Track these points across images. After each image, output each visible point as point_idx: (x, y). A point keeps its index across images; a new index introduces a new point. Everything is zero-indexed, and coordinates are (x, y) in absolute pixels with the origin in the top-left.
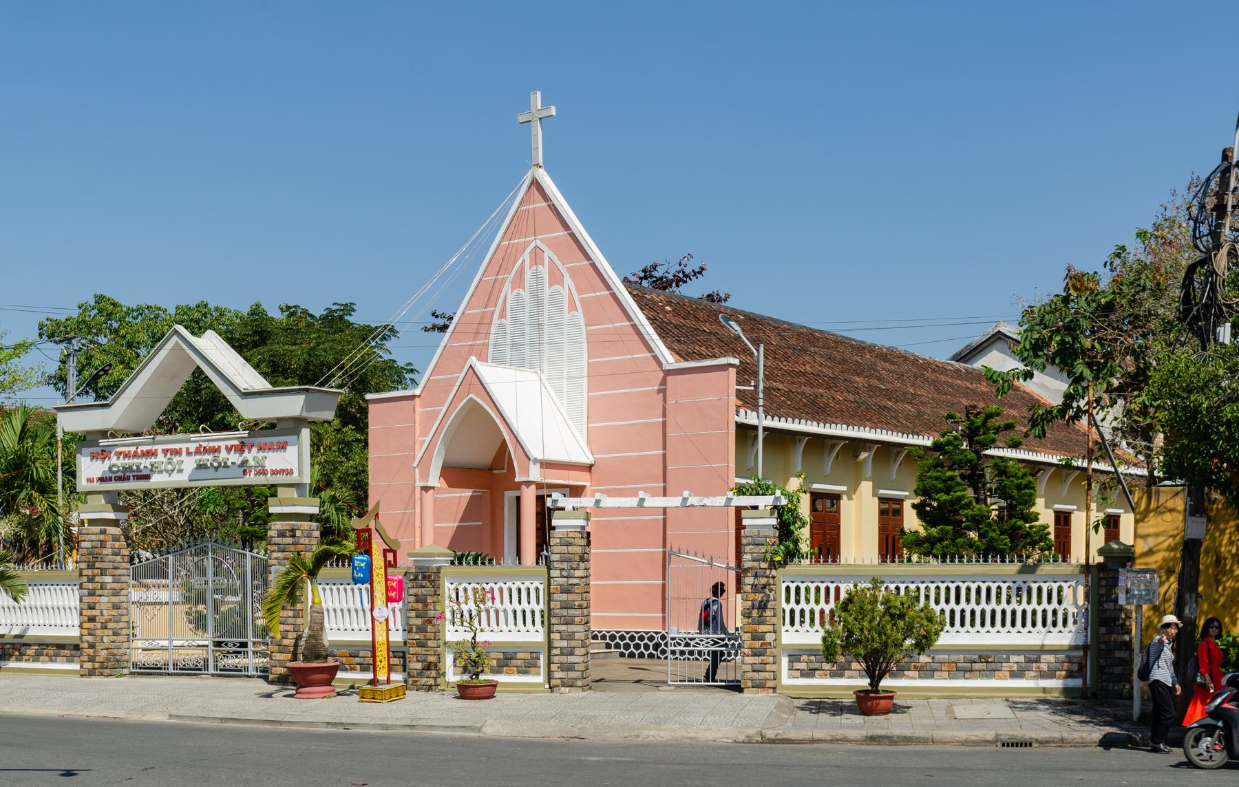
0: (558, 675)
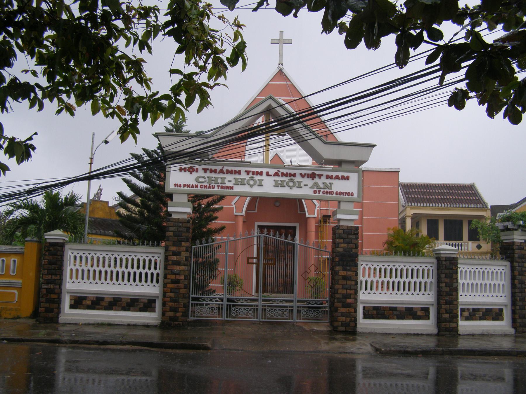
0: (519, 321)
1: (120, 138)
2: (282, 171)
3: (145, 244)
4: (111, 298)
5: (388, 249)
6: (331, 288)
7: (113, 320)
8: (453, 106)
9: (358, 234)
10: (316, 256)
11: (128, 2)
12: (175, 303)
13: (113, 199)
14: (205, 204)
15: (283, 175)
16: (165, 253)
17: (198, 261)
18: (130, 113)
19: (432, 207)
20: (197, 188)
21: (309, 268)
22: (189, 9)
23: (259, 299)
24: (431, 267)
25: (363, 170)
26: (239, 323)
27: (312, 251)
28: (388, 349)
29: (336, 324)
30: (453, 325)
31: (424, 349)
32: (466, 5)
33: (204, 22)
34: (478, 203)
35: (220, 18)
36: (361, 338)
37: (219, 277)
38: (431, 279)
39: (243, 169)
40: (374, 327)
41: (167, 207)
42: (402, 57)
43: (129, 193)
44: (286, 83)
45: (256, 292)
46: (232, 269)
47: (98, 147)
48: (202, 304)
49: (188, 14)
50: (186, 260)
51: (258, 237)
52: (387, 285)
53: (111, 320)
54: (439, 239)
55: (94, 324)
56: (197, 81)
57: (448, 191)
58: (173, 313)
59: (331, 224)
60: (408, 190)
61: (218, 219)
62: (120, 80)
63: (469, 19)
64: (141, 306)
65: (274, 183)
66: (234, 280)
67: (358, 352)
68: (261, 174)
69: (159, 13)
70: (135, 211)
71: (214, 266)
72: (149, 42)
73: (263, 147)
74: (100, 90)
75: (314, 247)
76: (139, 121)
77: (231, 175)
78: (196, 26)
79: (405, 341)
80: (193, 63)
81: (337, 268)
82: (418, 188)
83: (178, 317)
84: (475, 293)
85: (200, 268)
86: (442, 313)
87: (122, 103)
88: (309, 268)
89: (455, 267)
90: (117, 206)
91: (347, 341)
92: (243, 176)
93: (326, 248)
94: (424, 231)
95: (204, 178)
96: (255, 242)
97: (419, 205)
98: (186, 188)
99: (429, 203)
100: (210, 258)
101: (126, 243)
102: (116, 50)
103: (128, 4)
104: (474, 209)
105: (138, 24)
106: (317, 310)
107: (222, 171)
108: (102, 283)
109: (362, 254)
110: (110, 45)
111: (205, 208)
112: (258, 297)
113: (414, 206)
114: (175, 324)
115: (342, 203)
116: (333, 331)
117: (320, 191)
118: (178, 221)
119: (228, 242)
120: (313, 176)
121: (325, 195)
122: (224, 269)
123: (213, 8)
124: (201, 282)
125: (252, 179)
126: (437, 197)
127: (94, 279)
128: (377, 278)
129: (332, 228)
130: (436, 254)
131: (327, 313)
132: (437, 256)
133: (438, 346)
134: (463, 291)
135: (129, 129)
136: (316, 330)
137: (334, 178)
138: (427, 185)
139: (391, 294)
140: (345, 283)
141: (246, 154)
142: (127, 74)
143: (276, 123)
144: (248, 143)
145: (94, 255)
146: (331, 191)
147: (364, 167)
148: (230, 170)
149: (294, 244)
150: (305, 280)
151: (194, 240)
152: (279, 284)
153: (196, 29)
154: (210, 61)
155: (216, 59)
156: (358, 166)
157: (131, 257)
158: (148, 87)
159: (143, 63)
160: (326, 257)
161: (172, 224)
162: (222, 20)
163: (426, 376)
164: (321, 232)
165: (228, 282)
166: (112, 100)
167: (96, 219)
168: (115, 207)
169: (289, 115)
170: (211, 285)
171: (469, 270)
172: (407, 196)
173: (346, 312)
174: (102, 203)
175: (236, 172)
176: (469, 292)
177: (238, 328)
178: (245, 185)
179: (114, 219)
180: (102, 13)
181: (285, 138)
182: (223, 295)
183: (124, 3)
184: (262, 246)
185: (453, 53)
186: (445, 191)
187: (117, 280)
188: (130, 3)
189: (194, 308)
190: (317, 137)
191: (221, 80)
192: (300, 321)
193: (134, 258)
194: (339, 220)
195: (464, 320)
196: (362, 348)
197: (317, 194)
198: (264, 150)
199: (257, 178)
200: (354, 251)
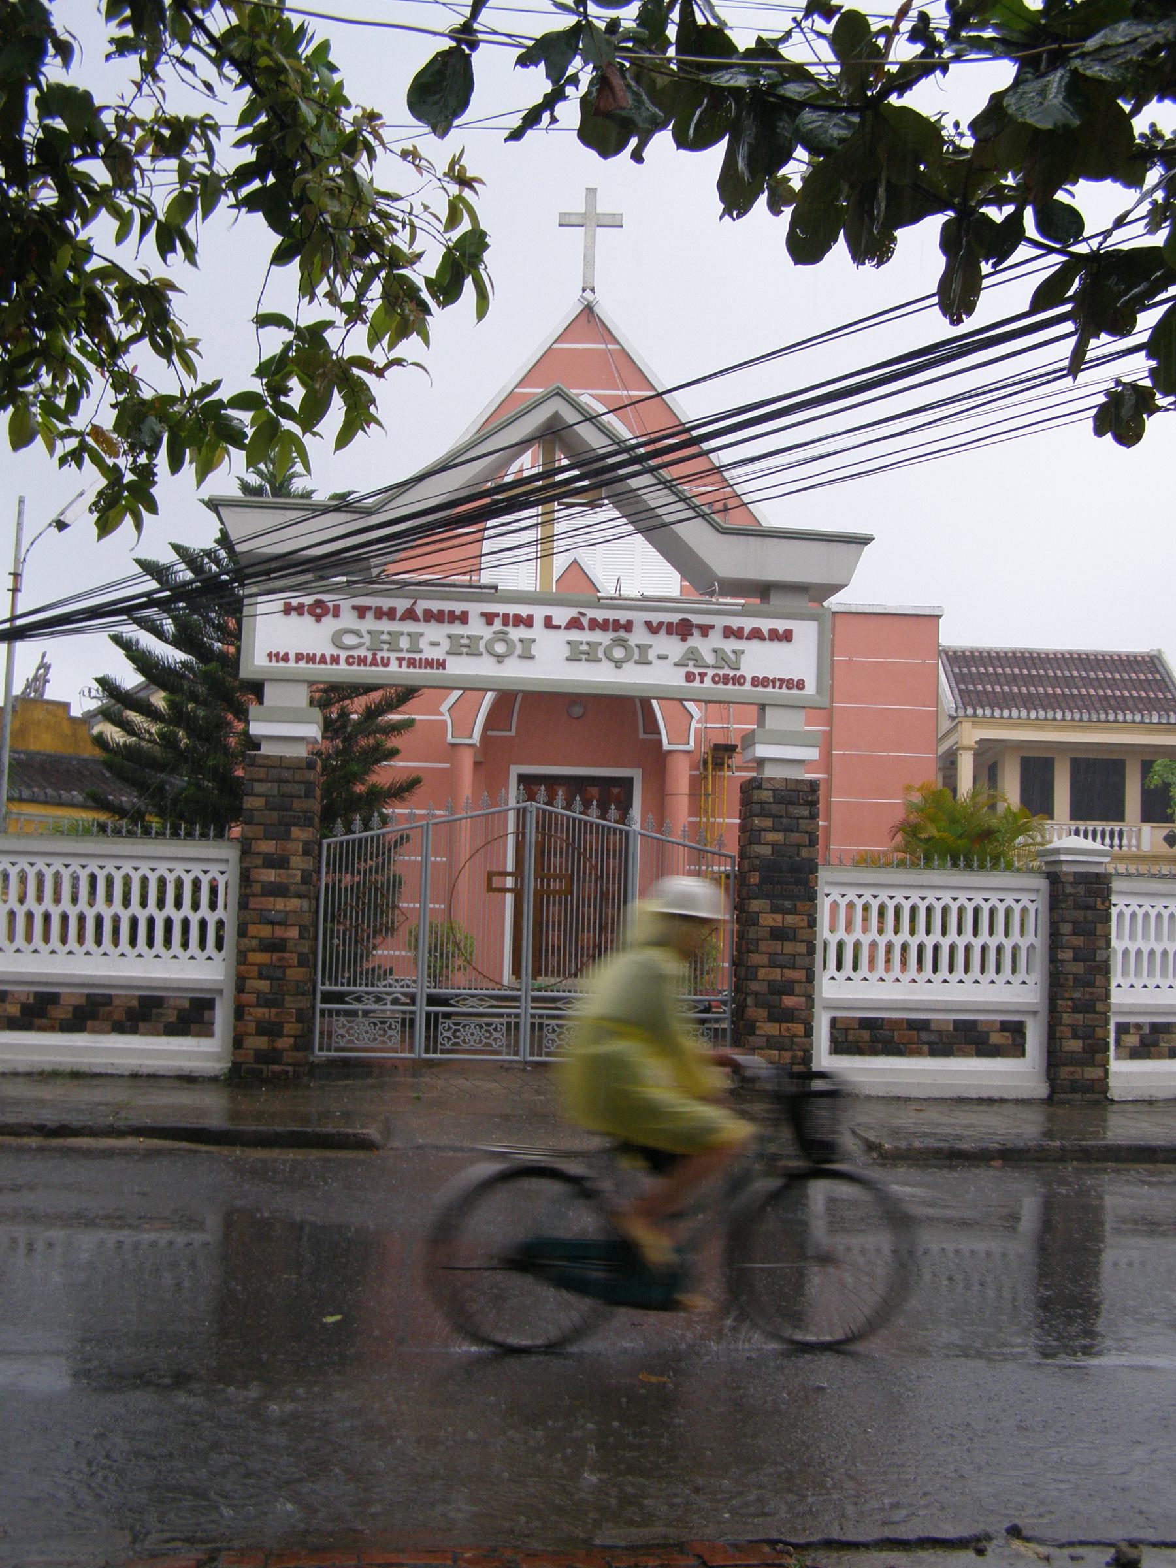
1: (98, 523)
2: (592, 613)
3: (182, 833)
4: (81, 995)
5: (906, 848)
6: (737, 963)
7: (86, 1060)
8: (1109, 435)
9: (817, 802)
11: (121, 103)
12: (274, 1011)
13: (82, 693)
14: (360, 711)
15: (594, 624)
16: (241, 861)
17: (340, 881)
18: (132, 447)
20: (338, 663)
24: (1032, 901)
25: (835, 609)
26: (463, 1069)
27: (681, 855)
28: (903, 1145)
30: (1093, 1073)
31: (1010, 1145)
32: (1153, 125)
33: (358, 169)
35: (405, 154)
37: (402, 934)
38: (1030, 938)
39: (475, 609)
41: (247, 722)
43: (129, 678)
45: (513, 974)
46: (443, 906)
48: (354, 1013)
51: (518, 811)
52: (902, 955)
53: (80, 1060)
55: (28, 1075)
56: (337, 353)
57: (1084, 674)
58: (266, 1039)
59: (737, 774)
60: (965, 670)
61: (398, 756)
63: (1160, 168)
65: (566, 651)
66: (448, 938)
68: (528, 622)
69: (218, 137)
70: (151, 734)
72: (190, 228)
74: (36, 375)
75: (687, 843)
76: (156, 475)
77: (440, 625)
78: (333, 184)
79: (953, 1121)
81: (755, 905)
82: (996, 663)
83: (282, 1051)
85: (346, 903)
86: (1061, 1039)
87: (107, 419)
89: (1103, 903)
90: (95, 716)
92: (476, 627)
93: (721, 844)
95: (357, 633)
96: (511, 827)
97: (997, 713)
98: (302, 664)
99: (1026, 708)
100: (377, 872)
101: (124, 830)
102: (87, 251)
103: (122, 112)
107: (410, 615)
108: (53, 952)
109: (827, 863)
110: (68, 237)
111: (359, 723)
112: (519, 990)
113: (984, 716)
114: (273, 1072)
115: (768, 710)
117: (705, 674)
120: (683, 630)
121: (721, 686)
122: (417, 905)
123: (383, 125)
124: (350, 945)
125: (501, 636)
126: (1050, 691)
127: (29, 938)
128: (873, 934)
130: (1046, 863)
131: (724, 1036)
132: (1051, 869)
133: (1049, 1134)
134: (1125, 973)
135: (125, 498)
137: (746, 634)
138: (1023, 653)
139: (914, 981)
141: (483, 566)
142: (122, 326)
143: (576, 472)
144: (488, 533)
145: (28, 868)
146: (738, 673)
147: (835, 602)
149: (627, 833)
151: (328, 817)
152: (582, 948)
154: (376, 289)
157: (140, 873)
159: (171, 294)
160: (722, 868)
161: (261, 773)
164: (707, 795)
166: (73, 405)
168: (89, 717)
169: (615, 447)
170: (380, 952)
171: (1143, 910)
172: (962, 686)
174: (50, 707)
175: (452, 618)
177: (460, 1081)
178: (480, 654)
180: (40, 135)
182: (414, 982)
183: (107, 108)
184: (532, 836)
185: (1113, 279)
186: (1075, 673)
187: (99, 942)
188: (127, 109)
189: (330, 1023)
190: (699, 516)
191: (410, 347)
193: (149, 874)
194: (761, 762)
197: (696, 684)
200: (804, 853)
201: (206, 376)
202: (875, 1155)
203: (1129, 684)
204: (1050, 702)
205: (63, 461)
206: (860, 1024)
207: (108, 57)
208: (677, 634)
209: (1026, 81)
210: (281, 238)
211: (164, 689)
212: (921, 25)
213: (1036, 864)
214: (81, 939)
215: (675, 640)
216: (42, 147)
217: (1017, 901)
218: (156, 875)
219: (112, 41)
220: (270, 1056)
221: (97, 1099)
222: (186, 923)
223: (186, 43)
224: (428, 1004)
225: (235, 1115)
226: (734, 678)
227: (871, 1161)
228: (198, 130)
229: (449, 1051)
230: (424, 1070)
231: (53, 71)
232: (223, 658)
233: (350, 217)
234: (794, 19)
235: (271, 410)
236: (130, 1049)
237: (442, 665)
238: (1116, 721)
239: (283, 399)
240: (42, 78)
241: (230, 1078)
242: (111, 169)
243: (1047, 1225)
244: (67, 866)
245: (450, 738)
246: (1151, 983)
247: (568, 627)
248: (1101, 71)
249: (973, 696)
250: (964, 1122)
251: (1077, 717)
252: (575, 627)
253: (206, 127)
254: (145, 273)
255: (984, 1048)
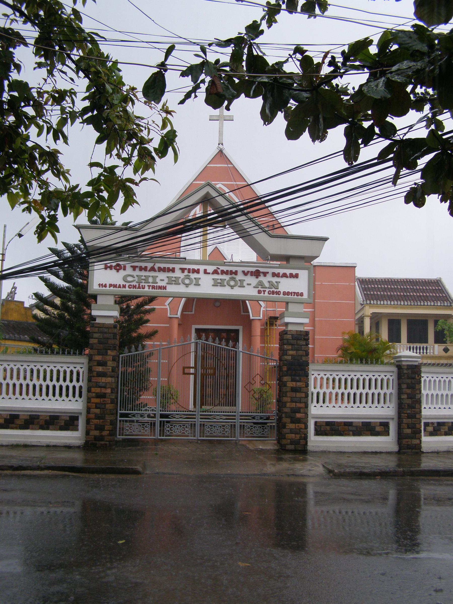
2: (222, 268)
3: (66, 353)
4: (28, 415)
6: (279, 401)
7: (30, 440)
8: (412, 203)
9: (308, 339)
10: (261, 363)
11: (39, 86)
12: (101, 420)
13: (29, 297)
15: (223, 272)
16: (89, 363)
17: (127, 370)
19: (393, 306)
20: (125, 288)
21: (253, 379)
22: (111, 94)
23: (197, 415)
26: (174, 442)
28: (342, 470)
29: (284, 442)
30: (415, 442)
31: (383, 470)
33: (128, 108)
34: (446, 301)
36: (312, 458)
37: (151, 390)
38: (390, 390)
39: (177, 267)
40: (327, 445)
41: (91, 310)
42: (353, 153)
43: (46, 292)
44: (226, 165)
47: (10, 241)
48: (133, 421)
49: (109, 99)
50: (113, 371)
54: (402, 342)
55: (7, 446)
57: (412, 287)
58: (98, 431)
60: (366, 286)
62: (32, 172)
63: (429, 105)
64: (62, 424)
65: (212, 282)
67: (309, 474)
68: (198, 271)
69: (76, 97)
70: (54, 314)
71: (145, 377)
72: (65, 129)
73: (200, 242)
75: (259, 355)
76: (57, 218)
80: (116, 155)
81: (285, 379)
82: (378, 283)
84: (440, 406)
85: (129, 379)
88: (253, 379)
89: (418, 376)
90: (34, 306)
91: (297, 462)
92: (178, 274)
93: (272, 355)
94: (384, 335)
97: (379, 303)
98: (112, 288)
99: (390, 300)
101: (44, 352)
103: (39, 90)
104: (441, 307)
105: (52, 110)
106: (263, 427)
107: (153, 269)
108: (17, 399)
109: (313, 362)
110: (19, 135)
113: (374, 304)
114: (101, 444)
115: (289, 304)
116: (281, 450)
117: (265, 291)
118: (103, 326)
119: (161, 350)
120: (257, 274)
121: (271, 295)
122: (156, 379)
125: (188, 277)
126: (399, 294)
128: (330, 389)
129: (279, 333)
130: (396, 361)
131: (274, 428)
133: (399, 466)
134: (427, 403)
136: (261, 449)
137: (281, 275)
138: (388, 280)
140: (294, 396)
141: (181, 251)
143: (216, 215)
144: (183, 238)
145: (7, 366)
146: (278, 290)
148: (162, 267)
149: (236, 351)
150: (249, 392)
151: (122, 346)
153: (119, 117)
154: (136, 153)
155: (143, 151)
156: (310, 262)
157: (50, 368)
158: (67, 180)
159: (59, 155)
160: (273, 364)
161: (96, 330)
162: (149, 106)
163: (385, 499)
164: (267, 336)
165: (161, 394)
167: (9, 322)
168: (32, 306)
169: (231, 206)
171: (433, 379)
172: (365, 292)
173: (295, 429)
175: (169, 270)
176: (433, 404)
177: (173, 447)
179: (30, 321)
180: (9, 98)
181: (226, 232)
182: (155, 408)
184: (200, 353)
185: (408, 149)
186: (408, 287)
188: (41, 89)
189: (123, 424)
190: (264, 231)
191: (149, 174)
192: (244, 439)
194: (287, 324)
195: (428, 436)
196: (313, 470)
197: (262, 294)
198: (202, 247)
199: (193, 276)
201: (73, 183)
202: (331, 475)
203: (429, 291)
204: (398, 298)
205: (24, 210)
206: (326, 424)
207: (35, 69)
208: (254, 276)
209: (371, 81)
210: (99, 134)
211: (60, 298)
212: (332, 61)
213: (392, 361)
214: (27, 394)
215: (254, 278)
216: (9, 102)
217: (385, 376)
218: (56, 369)
219: (36, 63)
220: (101, 438)
221: (33, 455)
222: (67, 387)
223: (64, 64)
224: (161, 418)
225: (86, 461)
226: (276, 292)
227: (330, 477)
228: (69, 94)
229: (169, 436)
230: (159, 443)
231: (14, 75)
232: (82, 285)
233: (125, 126)
234: (289, 55)
235: (96, 198)
236: (47, 436)
237: (165, 288)
238: (424, 305)
239: (101, 194)
240: (10, 78)
241: (84, 447)
242: (36, 110)
243: (399, 501)
244: (22, 366)
245: (169, 315)
246: (437, 407)
247: (213, 273)
248: (397, 78)
249: (370, 296)
250: (365, 461)
251: (409, 303)
252: (215, 273)
253: (72, 93)
254: (48, 147)
255: (374, 433)
